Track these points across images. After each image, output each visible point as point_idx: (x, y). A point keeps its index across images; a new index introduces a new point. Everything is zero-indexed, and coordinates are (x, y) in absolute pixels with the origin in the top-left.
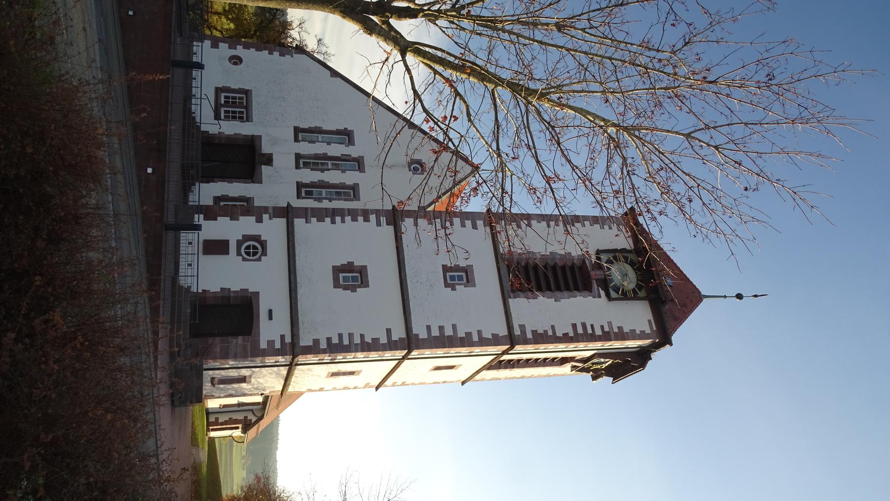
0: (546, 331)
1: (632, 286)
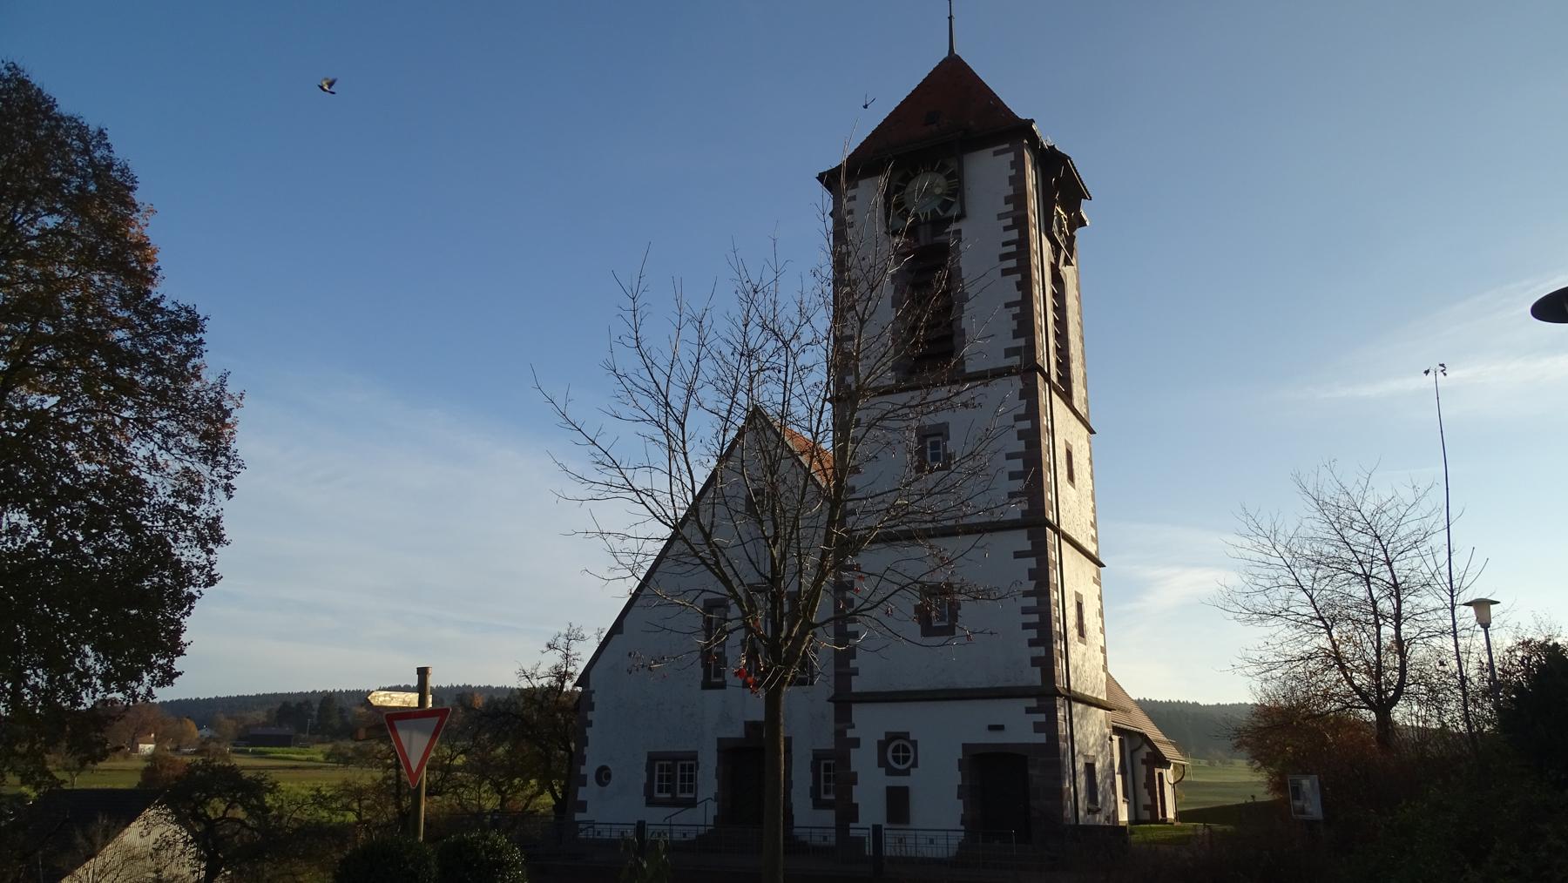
0: (1015, 317)
1: (940, 180)
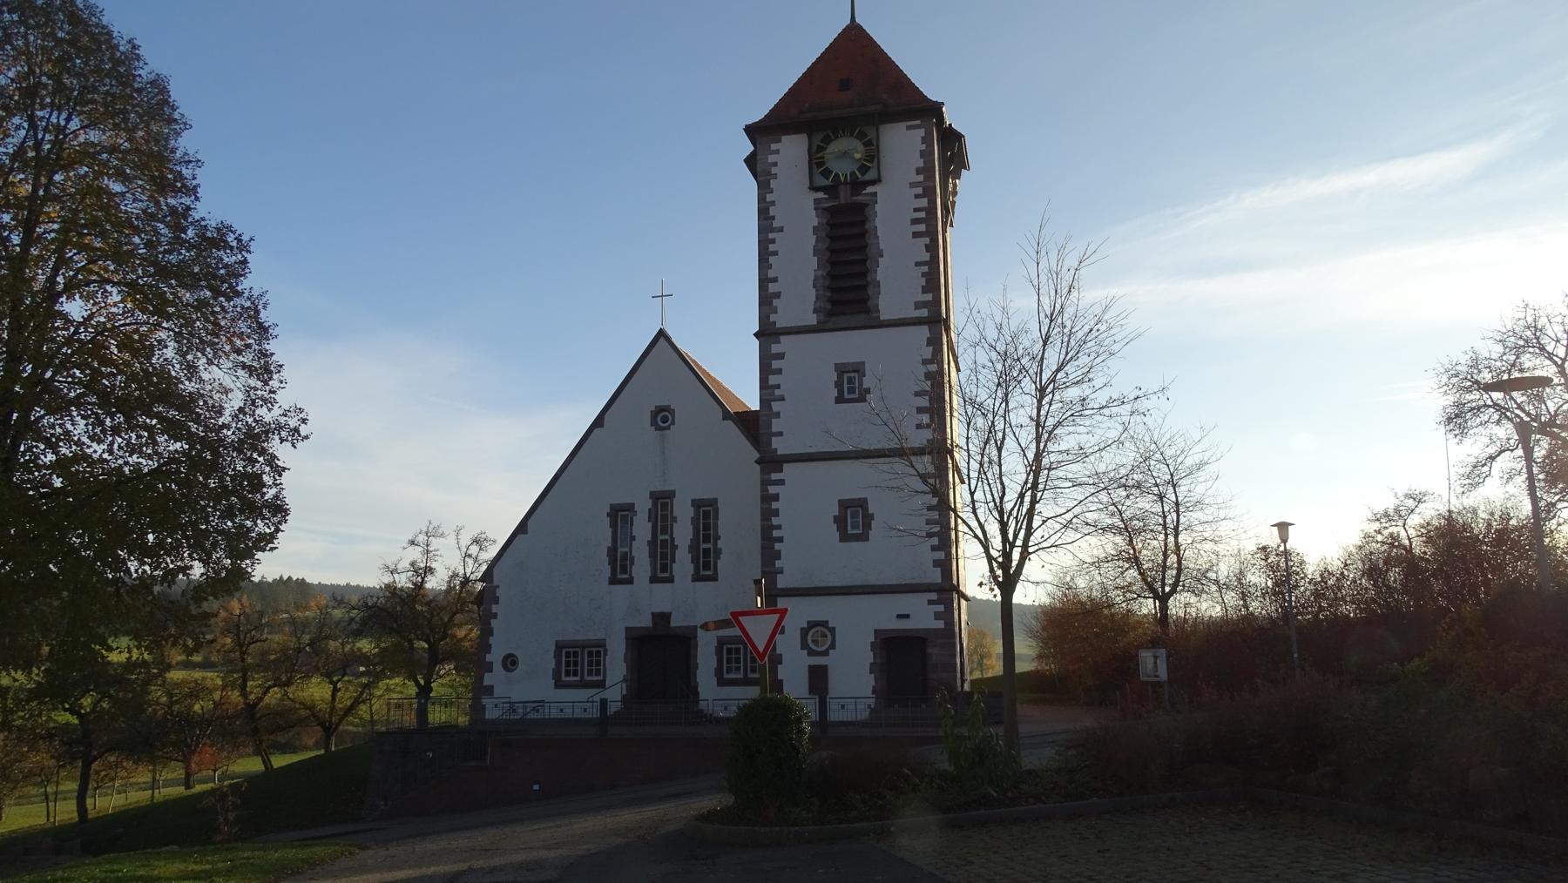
0: (923, 275)
